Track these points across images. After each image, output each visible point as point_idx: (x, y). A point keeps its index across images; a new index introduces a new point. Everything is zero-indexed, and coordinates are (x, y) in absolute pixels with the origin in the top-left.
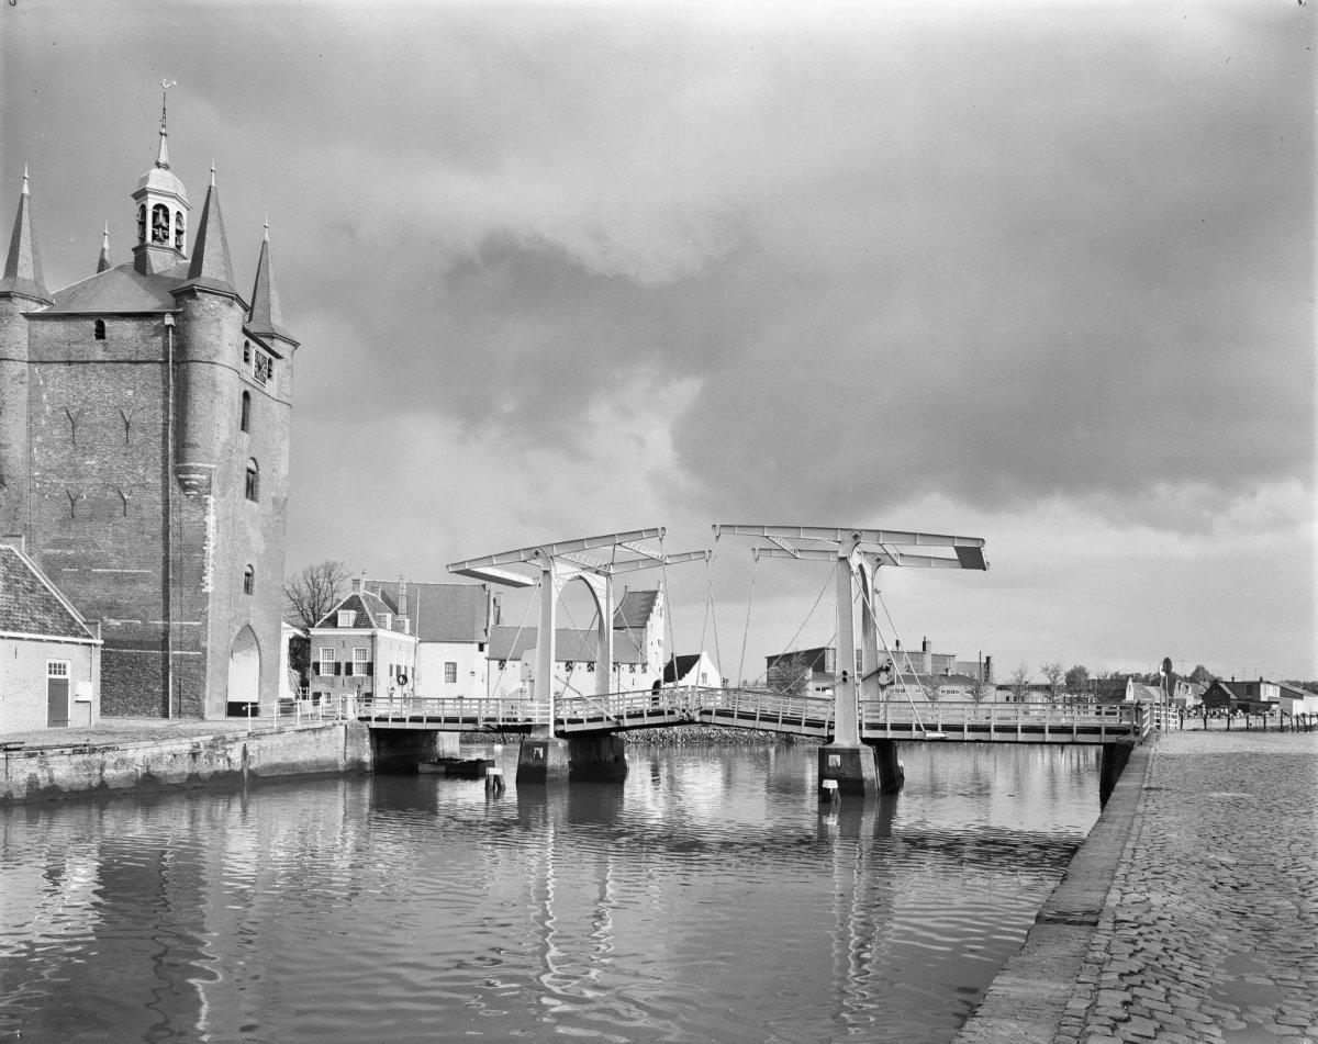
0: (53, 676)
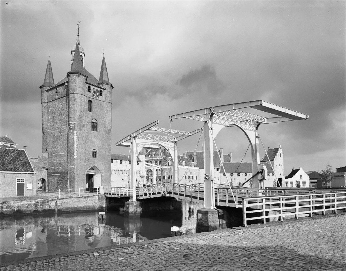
0: (19, 182)
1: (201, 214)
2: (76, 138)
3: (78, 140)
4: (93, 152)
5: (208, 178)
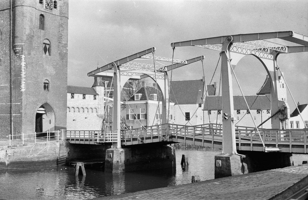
1: (221, 161)
2: (25, 64)
3: (27, 68)
4: (45, 83)
5: (227, 118)
